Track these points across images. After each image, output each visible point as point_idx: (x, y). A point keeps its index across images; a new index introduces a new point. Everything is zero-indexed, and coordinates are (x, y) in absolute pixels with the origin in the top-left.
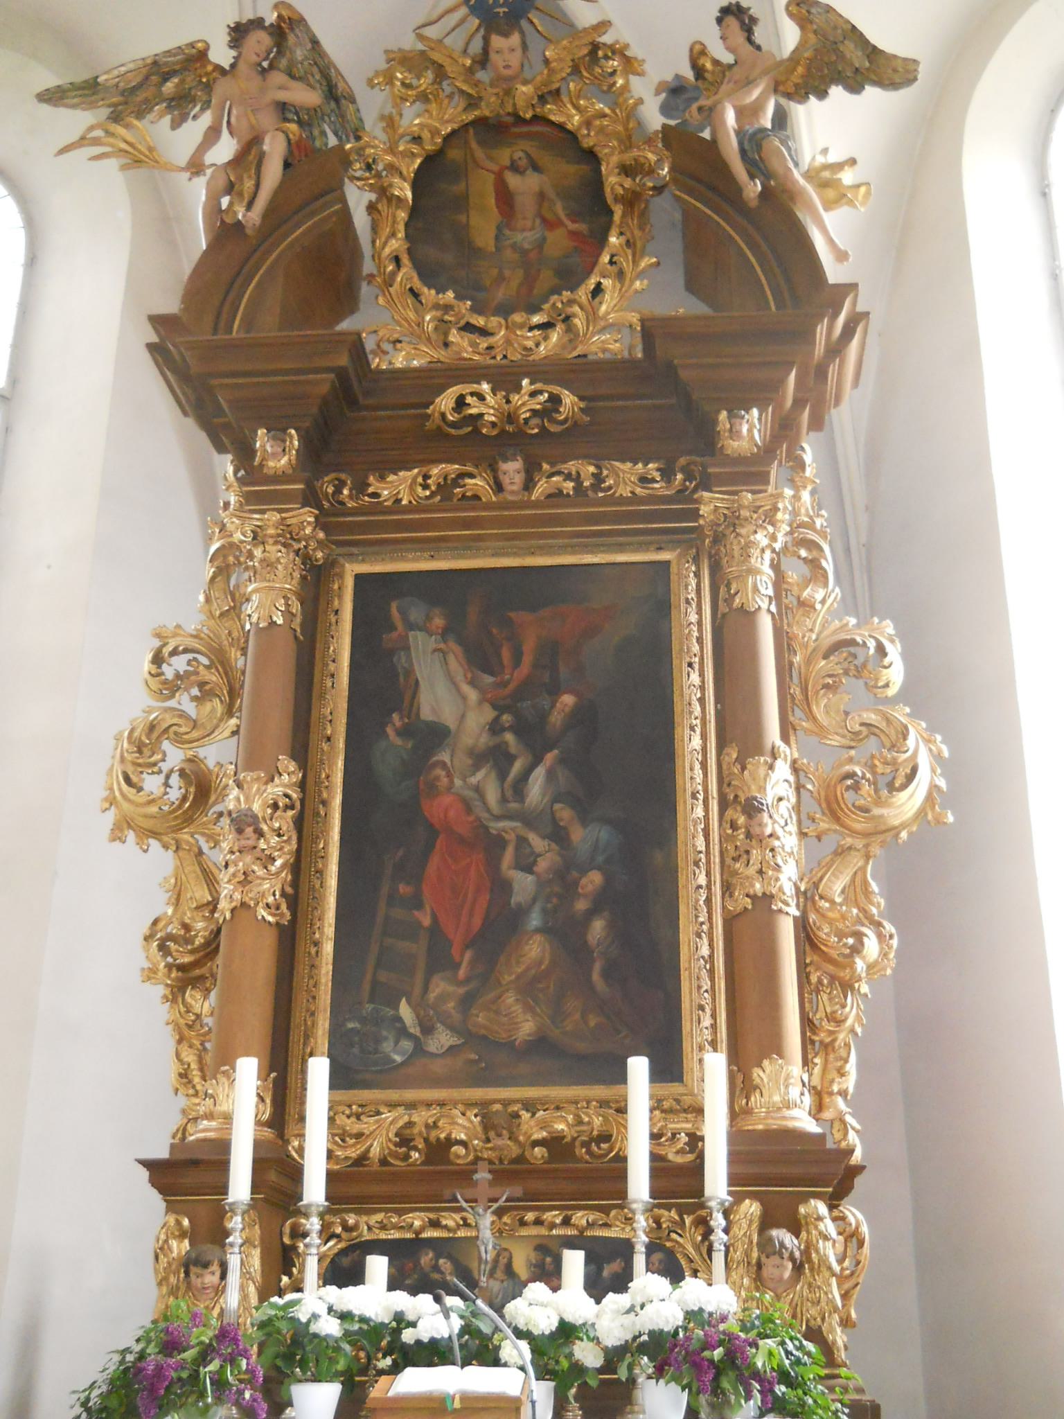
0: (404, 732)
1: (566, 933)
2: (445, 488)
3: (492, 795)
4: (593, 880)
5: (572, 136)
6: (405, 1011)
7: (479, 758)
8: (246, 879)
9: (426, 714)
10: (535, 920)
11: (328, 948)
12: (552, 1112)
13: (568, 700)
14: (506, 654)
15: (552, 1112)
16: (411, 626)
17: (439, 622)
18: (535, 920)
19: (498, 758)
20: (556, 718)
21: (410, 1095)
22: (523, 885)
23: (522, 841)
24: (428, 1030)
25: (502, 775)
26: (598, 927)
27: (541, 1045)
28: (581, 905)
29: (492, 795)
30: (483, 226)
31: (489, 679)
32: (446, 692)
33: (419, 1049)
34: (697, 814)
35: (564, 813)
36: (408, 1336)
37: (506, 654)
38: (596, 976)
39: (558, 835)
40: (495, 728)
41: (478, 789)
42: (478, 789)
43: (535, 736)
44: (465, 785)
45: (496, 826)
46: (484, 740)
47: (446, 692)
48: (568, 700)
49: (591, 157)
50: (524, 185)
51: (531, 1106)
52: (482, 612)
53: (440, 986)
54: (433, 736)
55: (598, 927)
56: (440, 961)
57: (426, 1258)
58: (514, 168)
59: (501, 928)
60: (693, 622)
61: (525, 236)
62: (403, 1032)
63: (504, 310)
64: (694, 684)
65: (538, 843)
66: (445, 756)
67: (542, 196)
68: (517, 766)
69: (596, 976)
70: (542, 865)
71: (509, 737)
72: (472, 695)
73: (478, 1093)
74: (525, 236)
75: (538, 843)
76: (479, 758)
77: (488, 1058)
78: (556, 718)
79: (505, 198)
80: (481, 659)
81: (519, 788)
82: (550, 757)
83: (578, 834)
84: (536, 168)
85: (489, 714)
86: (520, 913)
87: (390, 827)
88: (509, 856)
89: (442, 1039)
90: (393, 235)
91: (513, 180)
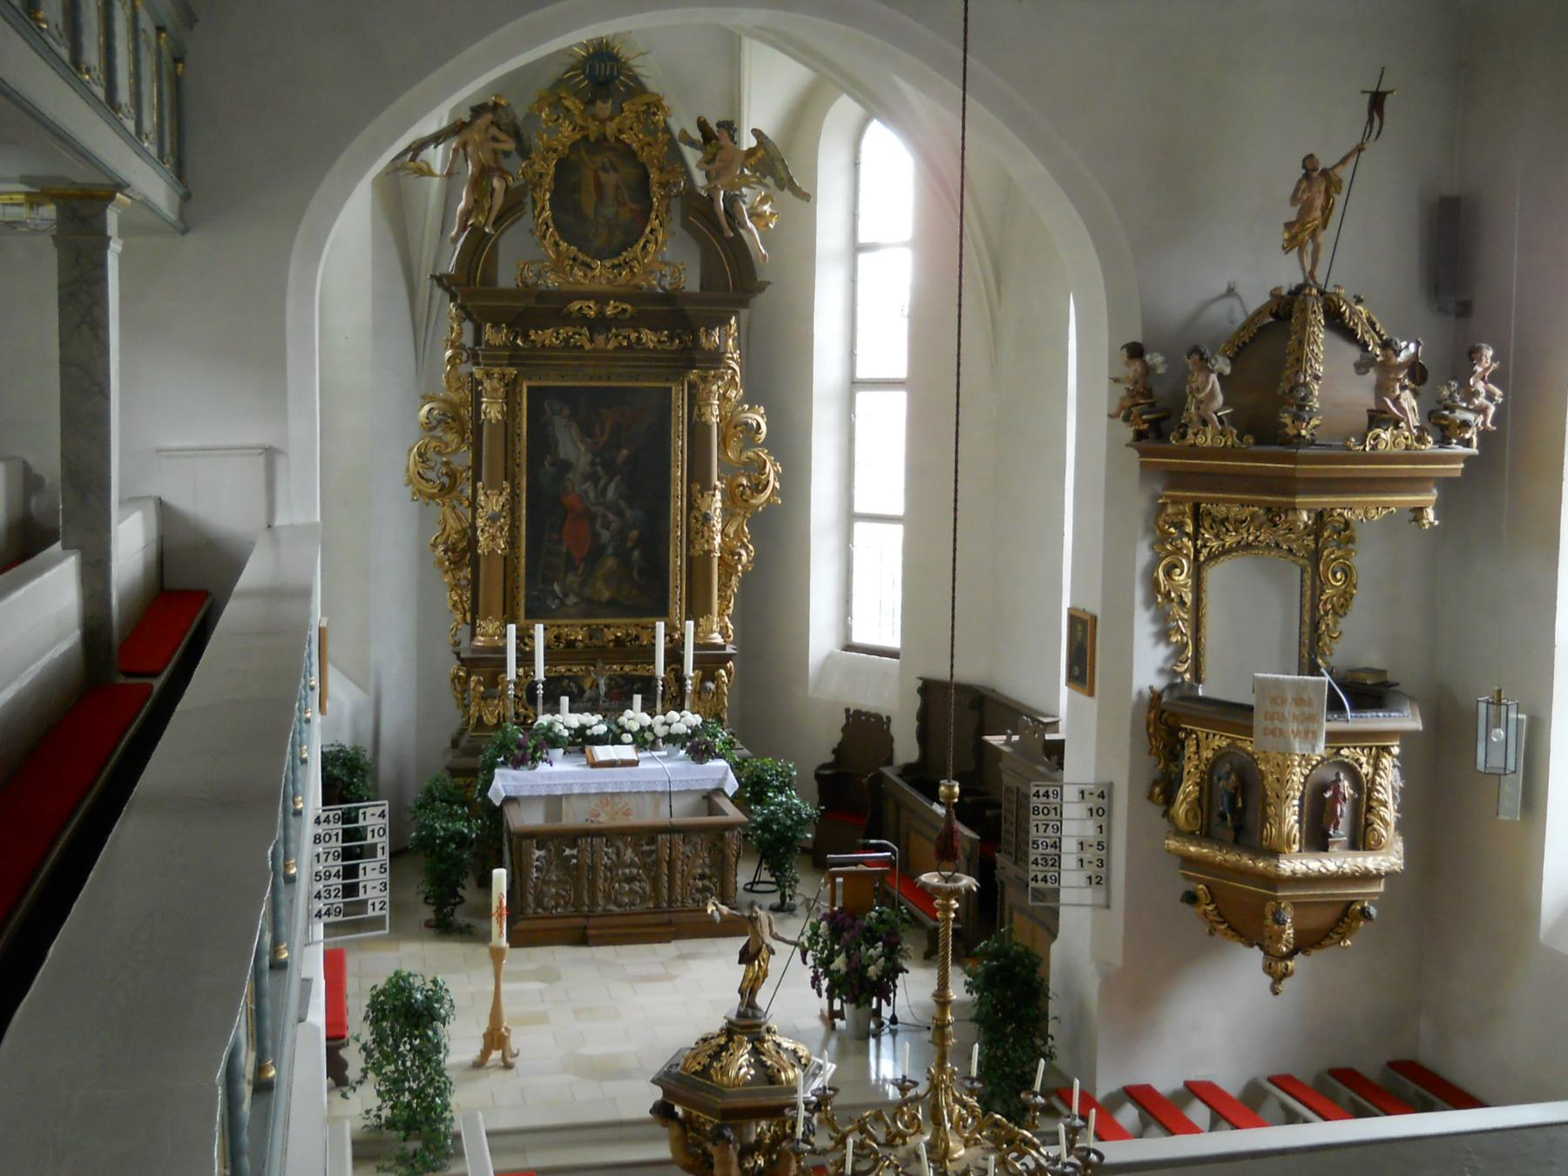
0: (553, 464)
1: (623, 556)
2: (567, 340)
3: (592, 494)
4: (634, 533)
5: (634, 153)
6: (556, 588)
7: (587, 477)
8: (494, 538)
9: (562, 455)
10: (610, 550)
11: (523, 561)
12: (617, 628)
13: (625, 452)
14: (598, 431)
15: (617, 628)
16: (554, 413)
17: (566, 412)
18: (610, 550)
19: (593, 478)
20: (620, 460)
21: (559, 622)
22: (605, 535)
23: (604, 516)
24: (566, 595)
25: (596, 486)
26: (636, 554)
27: (612, 602)
28: (630, 544)
29: (592, 494)
30: (588, 201)
31: (589, 440)
32: (571, 446)
33: (562, 604)
34: (678, 504)
35: (623, 504)
36: (589, 732)
37: (598, 431)
38: (635, 575)
39: (620, 513)
40: (593, 464)
41: (586, 492)
42: (586, 492)
43: (610, 468)
44: (579, 489)
45: (594, 509)
46: (588, 469)
47: (571, 446)
48: (625, 452)
49: (643, 168)
50: (609, 179)
51: (608, 626)
52: (587, 406)
53: (571, 578)
54: (566, 466)
55: (636, 554)
56: (570, 566)
57: (565, 683)
58: (604, 169)
59: (597, 553)
60: (680, 412)
61: (609, 211)
62: (555, 596)
63: (600, 256)
64: (679, 444)
65: (611, 516)
66: (570, 476)
67: (617, 187)
68: (602, 484)
69: (635, 575)
70: (613, 526)
71: (599, 469)
72: (583, 448)
73: (587, 621)
74: (609, 211)
75: (611, 516)
76: (587, 477)
77: (590, 607)
78: (620, 460)
79: (599, 186)
80: (586, 431)
81: (605, 489)
82: (617, 478)
83: (628, 514)
84: (616, 170)
85: (589, 457)
86: (603, 548)
87: (545, 510)
88: (599, 522)
89: (572, 600)
90: (543, 208)
91: (604, 177)
